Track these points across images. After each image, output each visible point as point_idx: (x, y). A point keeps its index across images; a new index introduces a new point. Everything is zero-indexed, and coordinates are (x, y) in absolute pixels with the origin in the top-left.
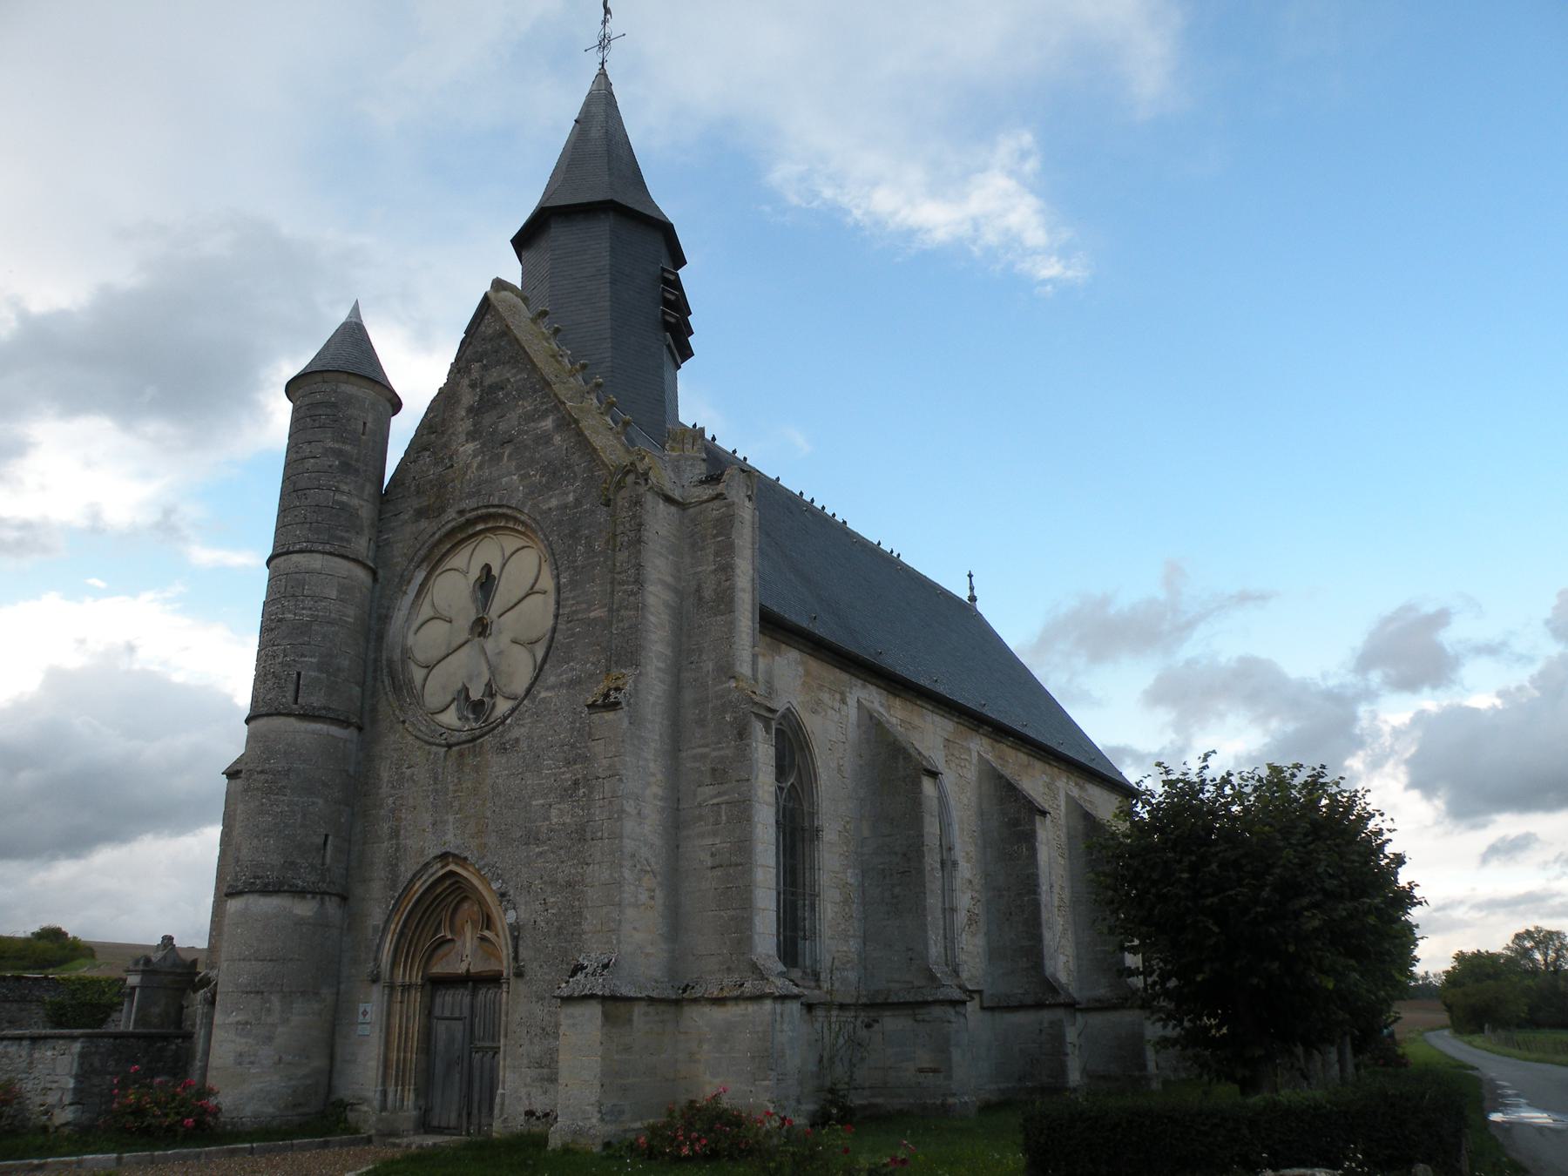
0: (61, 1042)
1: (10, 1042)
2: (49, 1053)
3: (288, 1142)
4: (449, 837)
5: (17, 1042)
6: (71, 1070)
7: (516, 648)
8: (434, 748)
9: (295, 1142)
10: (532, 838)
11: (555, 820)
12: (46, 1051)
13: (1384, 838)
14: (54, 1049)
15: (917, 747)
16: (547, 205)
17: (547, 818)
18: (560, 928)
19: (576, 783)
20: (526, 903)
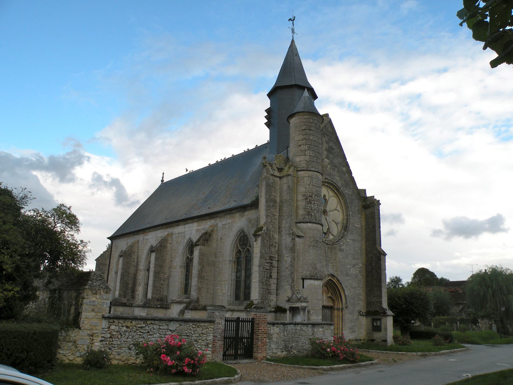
0: (325, 326)
1: (302, 326)
2: (321, 329)
3: (293, 366)
4: (330, 270)
5: (306, 325)
6: (332, 334)
7: (333, 223)
8: (324, 244)
9: (295, 366)
10: (347, 275)
11: (352, 272)
12: (320, 328)
13: (34, 302)
14: (323, 328)
15: (277, 264)
16: (277, 86)
17: (350, 271)
18: (353, 297)
19: (355, 264)
20: (347, 290)
